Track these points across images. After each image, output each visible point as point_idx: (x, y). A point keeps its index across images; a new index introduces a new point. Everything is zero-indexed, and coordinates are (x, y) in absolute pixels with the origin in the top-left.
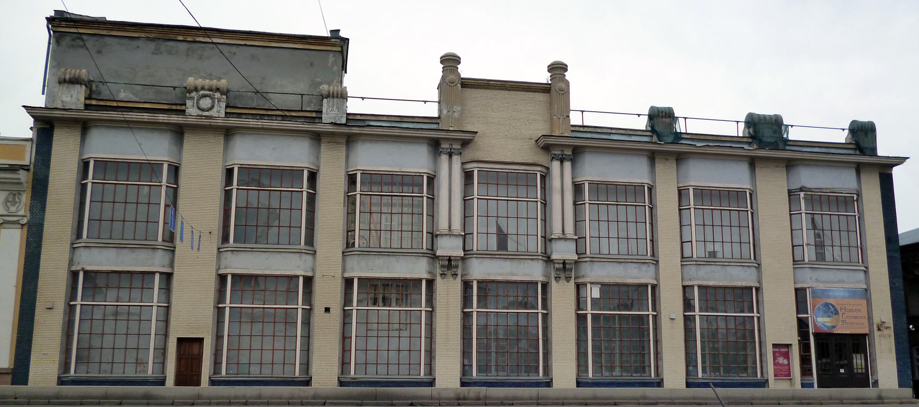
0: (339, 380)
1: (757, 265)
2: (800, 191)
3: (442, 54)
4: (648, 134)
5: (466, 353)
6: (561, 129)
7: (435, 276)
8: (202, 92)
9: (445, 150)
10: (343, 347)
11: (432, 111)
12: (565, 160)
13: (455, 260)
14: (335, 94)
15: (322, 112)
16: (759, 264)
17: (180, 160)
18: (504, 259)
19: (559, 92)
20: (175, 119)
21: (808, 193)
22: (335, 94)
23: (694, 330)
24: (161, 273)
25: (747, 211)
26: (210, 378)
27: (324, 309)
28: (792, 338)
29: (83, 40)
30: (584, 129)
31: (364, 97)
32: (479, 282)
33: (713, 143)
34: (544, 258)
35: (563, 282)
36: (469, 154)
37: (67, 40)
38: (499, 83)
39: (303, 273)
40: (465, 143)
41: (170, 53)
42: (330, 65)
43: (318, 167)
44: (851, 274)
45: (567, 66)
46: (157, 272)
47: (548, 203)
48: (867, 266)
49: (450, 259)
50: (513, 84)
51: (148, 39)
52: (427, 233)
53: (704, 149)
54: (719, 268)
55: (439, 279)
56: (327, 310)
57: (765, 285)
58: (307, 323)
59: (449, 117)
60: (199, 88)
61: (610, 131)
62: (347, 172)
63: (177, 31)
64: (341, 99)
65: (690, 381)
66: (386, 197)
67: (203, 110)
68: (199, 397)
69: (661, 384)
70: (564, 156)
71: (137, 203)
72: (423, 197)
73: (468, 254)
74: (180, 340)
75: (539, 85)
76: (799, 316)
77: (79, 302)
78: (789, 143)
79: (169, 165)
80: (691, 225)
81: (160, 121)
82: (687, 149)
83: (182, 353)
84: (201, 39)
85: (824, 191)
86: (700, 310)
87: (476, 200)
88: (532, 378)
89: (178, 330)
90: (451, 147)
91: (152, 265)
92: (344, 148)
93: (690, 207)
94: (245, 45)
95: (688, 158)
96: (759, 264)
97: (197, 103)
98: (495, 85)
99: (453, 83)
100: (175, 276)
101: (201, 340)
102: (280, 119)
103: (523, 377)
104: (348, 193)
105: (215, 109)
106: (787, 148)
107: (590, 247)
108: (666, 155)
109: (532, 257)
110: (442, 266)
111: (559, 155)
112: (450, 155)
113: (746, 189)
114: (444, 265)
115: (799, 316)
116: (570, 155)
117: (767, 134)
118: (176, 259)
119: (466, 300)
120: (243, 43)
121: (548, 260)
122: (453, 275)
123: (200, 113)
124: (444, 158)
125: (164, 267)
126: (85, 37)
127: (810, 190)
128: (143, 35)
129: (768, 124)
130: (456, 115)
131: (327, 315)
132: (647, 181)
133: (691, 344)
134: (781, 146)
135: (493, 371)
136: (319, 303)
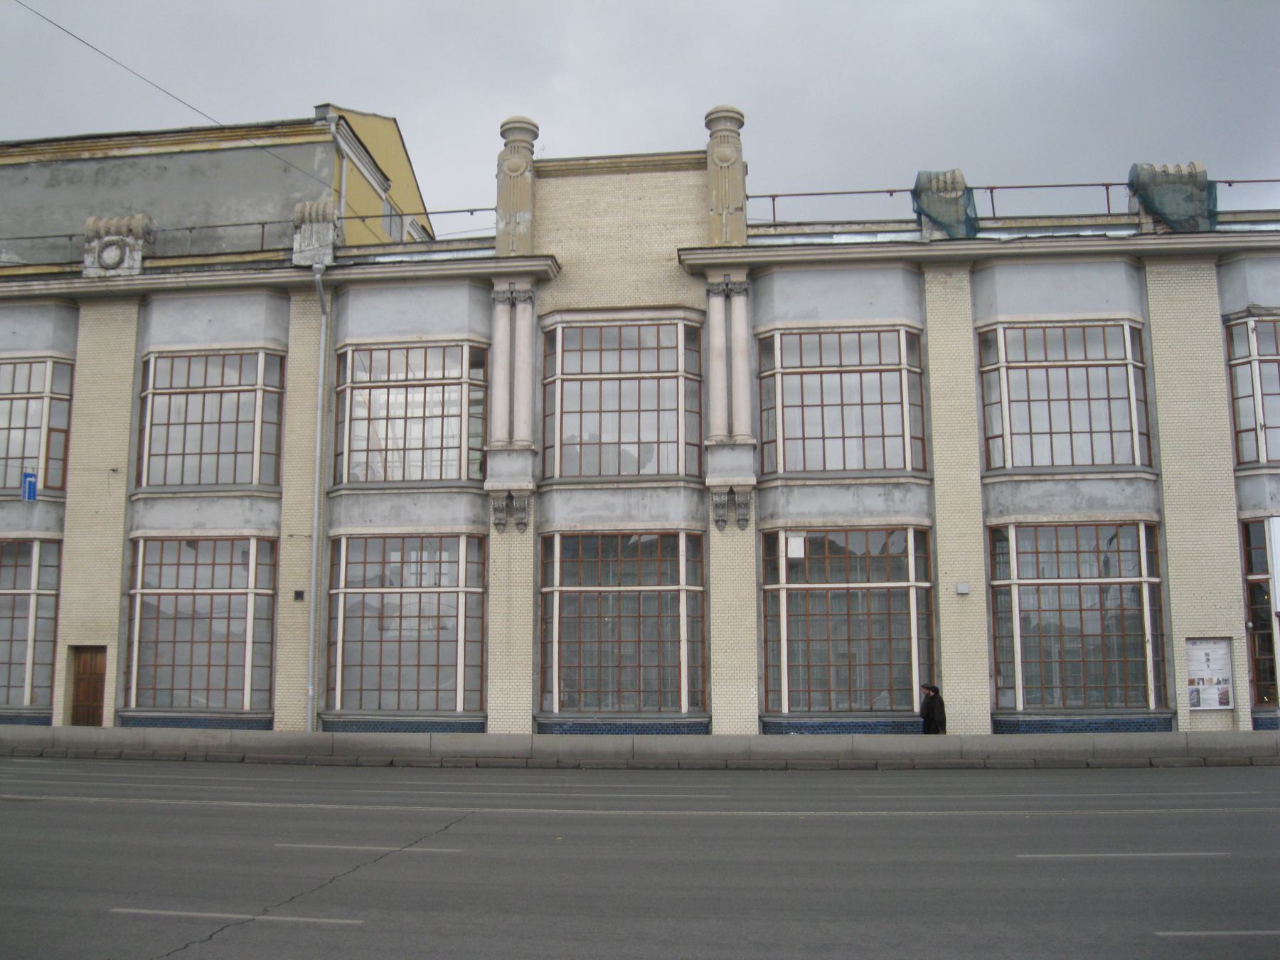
0: (992, 718)
1: (1153, 477)
2: (1248, 316)
4: (912, 226)
6: (724, 233)
7: (707, 526)
8: (107, 239)
9: (500, 296)
10: (995, 659)
11: (486, 225)
12: (732, 294)
13: (520, 497)
14: (314, 215)
15: (292, 249)
16: (1157, 475)
17: (924, 321)
18: (612, 491)
19: (720, 164)
21: (1265, 318)
22: (314, 215)
23: (920, 616)
24: (260, 539)
25: (1126, 365)
26: (760, 717)
27: (293, 594)
30: (776, 230)
31: (993, 185)
32: (564, 537)
33: (1019, 233)
34: (692, 485)
35: (732, 530)
36: (550, 297)
38: (607, 161)
39: (255, 533)
40: (541, 280)
41: (71, 181)
42: (316, 167)
43: (287, 345)
45: (742, 116)
46: (253, 536)
47: (703, 379)
48: (1158, 472)
49: (510, 497)
50: (634, 159)
51: (40, 163)
52: (686, 444)
53: (1019, 245)
54: (1062, 486)
55: (494, 534)
56: (299, 595)
57: (1169, 518)
59: (509, 234)
60: (103, 232)
61: (829, 229)
62: (336, 350)
63: (78, 144)
64: (325, 224)
65: (541, 720)
66: (610, 382)
67: (107, 268)
68: (54, 743)
69: (1174, 723)
70: (730, 286)
71: (822, 406)
72: (677, 377)
73: (543, 486)
74: (77, 650)
75: (681, 157)
76: (1251, 577)
77: (556, 587)
78: (1220, 218)
79: (266, 354)
80: (1253, 396)
81: (170, 285)
82: (1119, 245)
83: (81, 671)
84: (116, 152)
86: (788, 582)
87: (778, 377)
88: (667, 718)
89: (70, 635)
90: (727, 281)
91: (28, 528)
93: (256, 387)
94: (182, 152)
95: (1244, 259)
96: (1157, 475)
97: (99, 256)
98: (601, 166)
99: (727, 161)
100: (65, 541)
101: (102, 649)
102: (194, 270)
103: (649, 718)
104: (336, 388)
105: (126, 265)
106: (1219, 228)
107: (787, 457)
108: (947, 264)
109: (662, 481)
110: (496, 510)
111: (719, 284)
112: (513, 305)
113: (1122, 319)
114: (499, 508)
115: (1251, 577)
116: (741, 283)
117: (1174, 205)
118: (67, 518)
120: (177, 149)
121: (698, 483)
122: (518, 524)
123: (102, 273)
124: (502, 311)
125: (47, 529)
128: (32, 158)
129: (1174, 183)
130: (522, 229)
131: (299, 604)
132: (1127, 315)
133: (475, 684)
134: (1204, 224)
135: (1056, 700)
136: (288, 582)
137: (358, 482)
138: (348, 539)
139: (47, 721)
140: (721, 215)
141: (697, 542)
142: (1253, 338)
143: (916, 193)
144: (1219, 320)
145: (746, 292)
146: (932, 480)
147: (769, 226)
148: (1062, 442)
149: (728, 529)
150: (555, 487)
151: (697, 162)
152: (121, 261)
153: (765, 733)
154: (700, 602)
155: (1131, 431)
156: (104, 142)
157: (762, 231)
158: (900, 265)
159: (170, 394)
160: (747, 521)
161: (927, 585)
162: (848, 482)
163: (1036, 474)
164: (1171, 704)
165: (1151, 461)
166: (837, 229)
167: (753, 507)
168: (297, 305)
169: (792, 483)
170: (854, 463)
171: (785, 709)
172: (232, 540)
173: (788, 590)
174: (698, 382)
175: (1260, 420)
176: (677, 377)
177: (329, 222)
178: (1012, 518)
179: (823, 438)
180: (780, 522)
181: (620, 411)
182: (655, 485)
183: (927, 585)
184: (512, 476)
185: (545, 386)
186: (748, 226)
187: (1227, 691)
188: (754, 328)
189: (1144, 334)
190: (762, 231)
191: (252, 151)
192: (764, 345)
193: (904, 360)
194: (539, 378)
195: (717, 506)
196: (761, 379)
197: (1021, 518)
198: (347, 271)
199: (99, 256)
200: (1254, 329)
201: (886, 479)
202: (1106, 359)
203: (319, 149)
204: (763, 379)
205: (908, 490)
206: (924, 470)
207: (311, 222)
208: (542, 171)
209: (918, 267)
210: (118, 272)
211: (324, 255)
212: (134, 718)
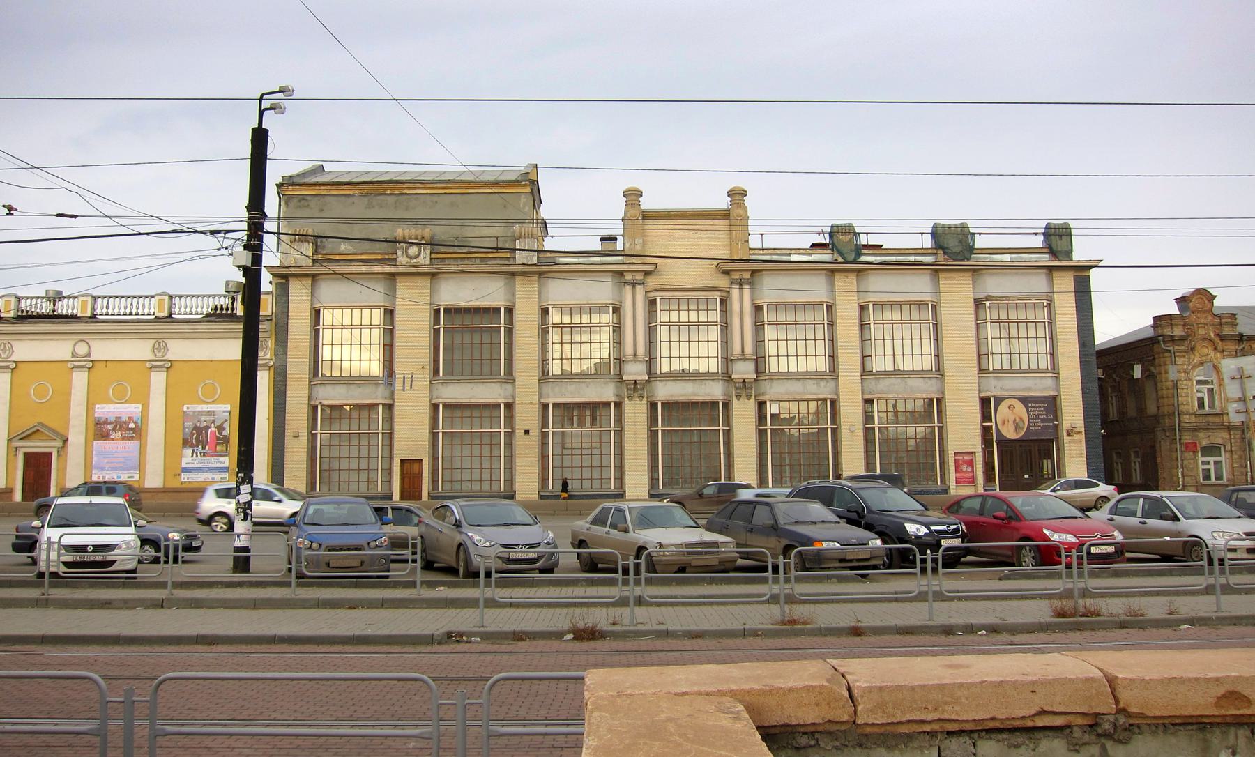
3: (624, 189)
5: (653, 468)
20: (388, 269)
24: (384, 405)
28: (976, 445)
29: (306, 200)
36: (651, 280)
37: (294, 202)
39: (503, 400)
40: (647, 273)
43: (514, 303)
44: (1038, 381)
45: (746, 192)
49: (635, 383)
54: (899, 380)
56: (527, 432)
58: (510, 445)
61: (789, 252)
67: (411, 258)
72: (929, 323)
77: (660, 428)
78: (975, 252)
84: (407, 191)
85: (1011, 299)
88: (931, 487)
89: (400, 453)
92: (855, 278)
94: (445, 193)
97: (406, 252)
105: (422, 256)
111: (737, 279)
112: (741, 285)
117: (952, 243)
119: (653, 420)
120: (443, 192)
121: (619, 378)
125: (386, 398)
126: (309, 198)
127: (996, 299)
128: (356, 192)
131: (527, 437)
137: (899, 370)
138: (443, 405)
139: (390, 498)
140: (738, 244)
141: (726, 405)
142: (988, 310)
143: (933, 234)
144: (973, 301)
145: (750, 283)
146: (838, 376)
147: (760, 249)
148: (792, 360)
149: (742, 399)
150: (659, 379)
151: (724, 215)
152: (419, 254)
153: (401, 500)
154: (728, 433)
155: (931, 355)
156: (401, 185)
157: (756, 252)
158: (611, 274)
159: (352, 328)
160: (751, 395)
161: (835, 426)
162: (799, 377)
163: (788, 375)
164: (947, 483)
165: (1054, 367)
166: (793, 252)
167: (753, 389)
168: (519, 282)
169: (773, 378)
170: (802, 368)
171: (661, 487)
172: (704, 403)
173: (771, 429)
174: (725, 326)
175: (990, 351)
176: (609, 326)
177: (535, 238)
178: (876, 396)
179: (778, 356)
180: (767, 397)
181: (679, 341)
182: (707, 378)
183: (835, 426)
184: (637, 374)
185: (651, 329)
186: (750, 249)
187: (216, 490)
188: (753, 300)
189: (938, 308)
190: (756, 252)
191: (343, 198)
192: (758, 309)
193: (825, 319)
194: (647, 322)
195: (737, 388)
196: (756, 326)
197: (879, 396)
198: (551, 267)
199: (406, 252)
200: (989, 307)
201: (816, 375)
202: (1017, 319)
203: (523, 196)
204: (758, 327)
205: (827, 382)
206: (834, 372)
207: (525, 238)
208: (647, 216)
209: (1050, 269)
210: (418, 260)
211: (533, 256)
212: (442, 496)
